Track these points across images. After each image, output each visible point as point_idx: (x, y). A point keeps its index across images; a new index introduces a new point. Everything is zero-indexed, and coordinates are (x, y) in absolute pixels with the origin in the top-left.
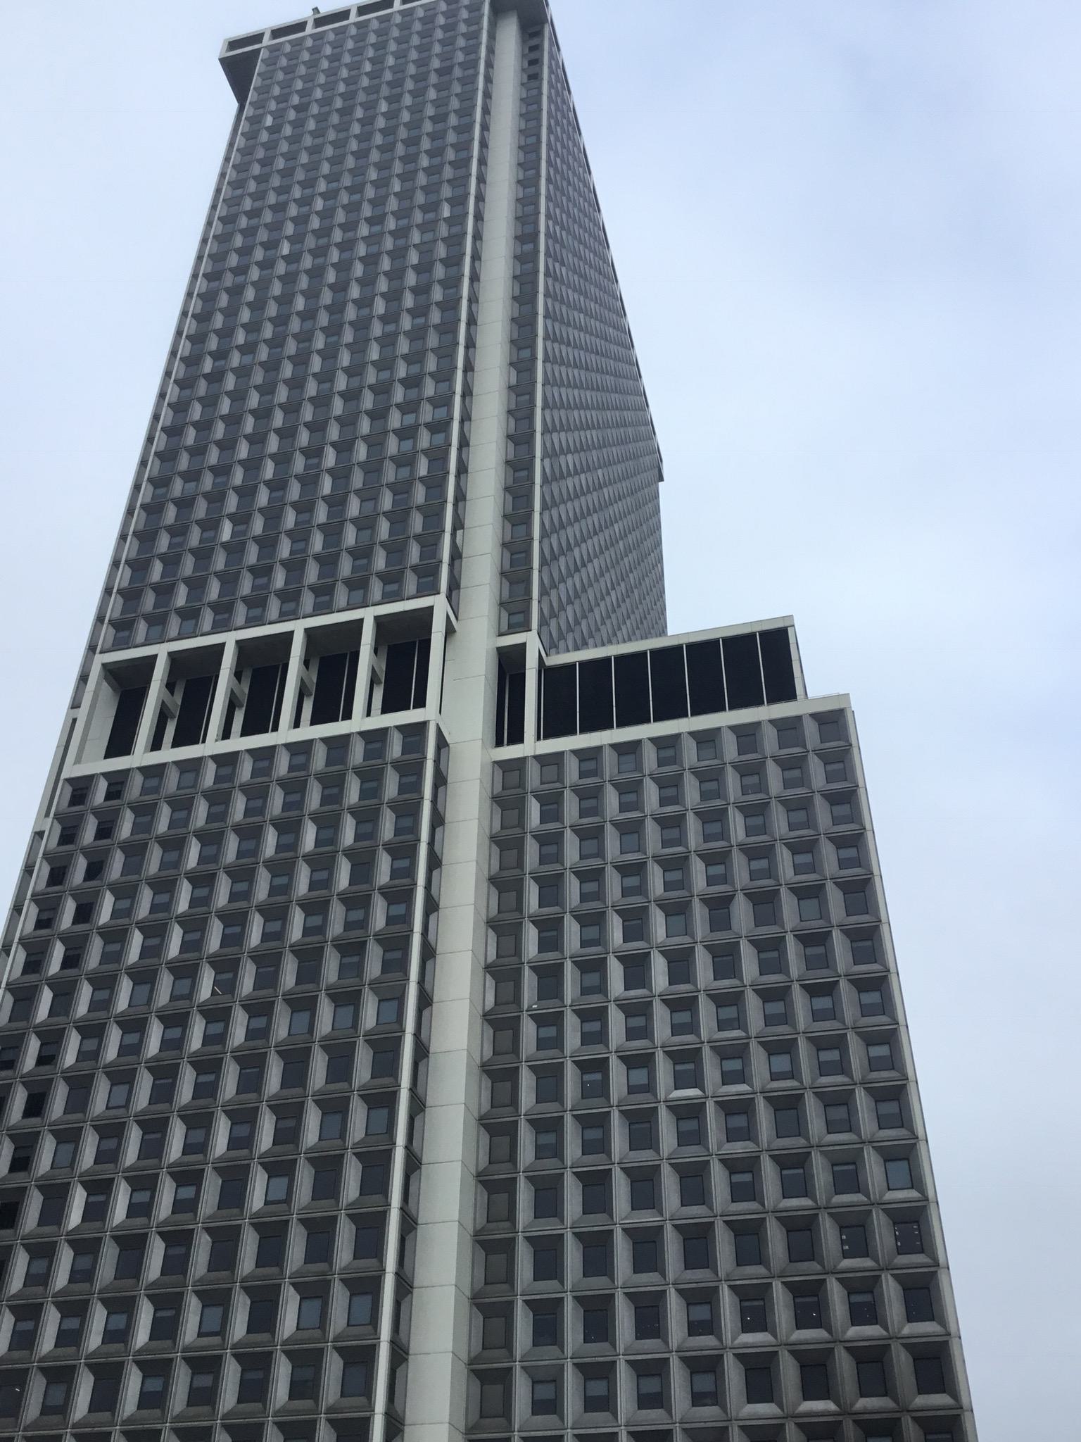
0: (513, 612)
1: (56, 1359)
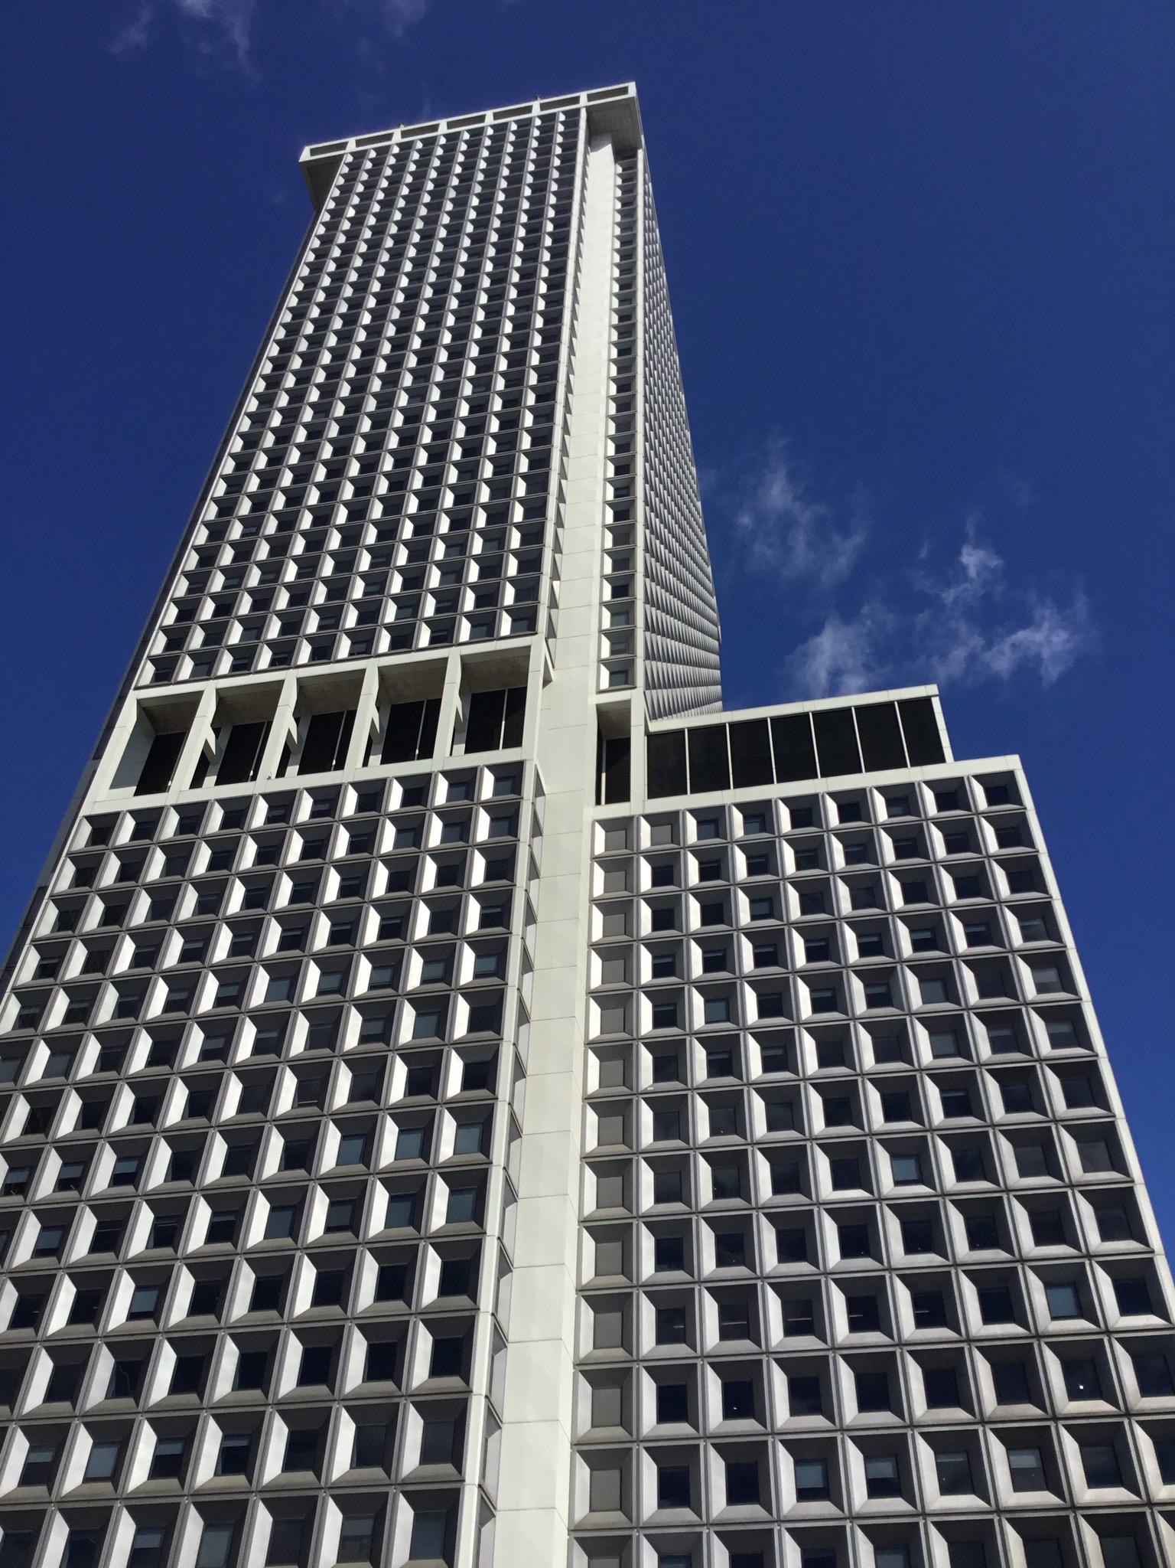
1: (213, 1485)
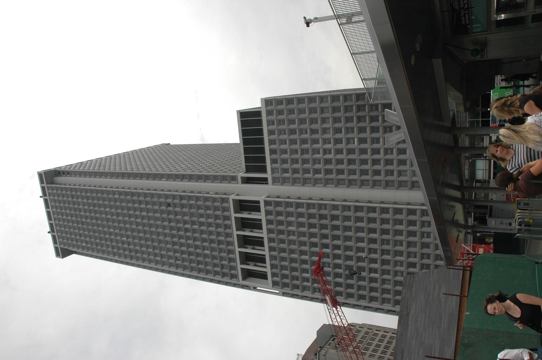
0: (233, 179)
